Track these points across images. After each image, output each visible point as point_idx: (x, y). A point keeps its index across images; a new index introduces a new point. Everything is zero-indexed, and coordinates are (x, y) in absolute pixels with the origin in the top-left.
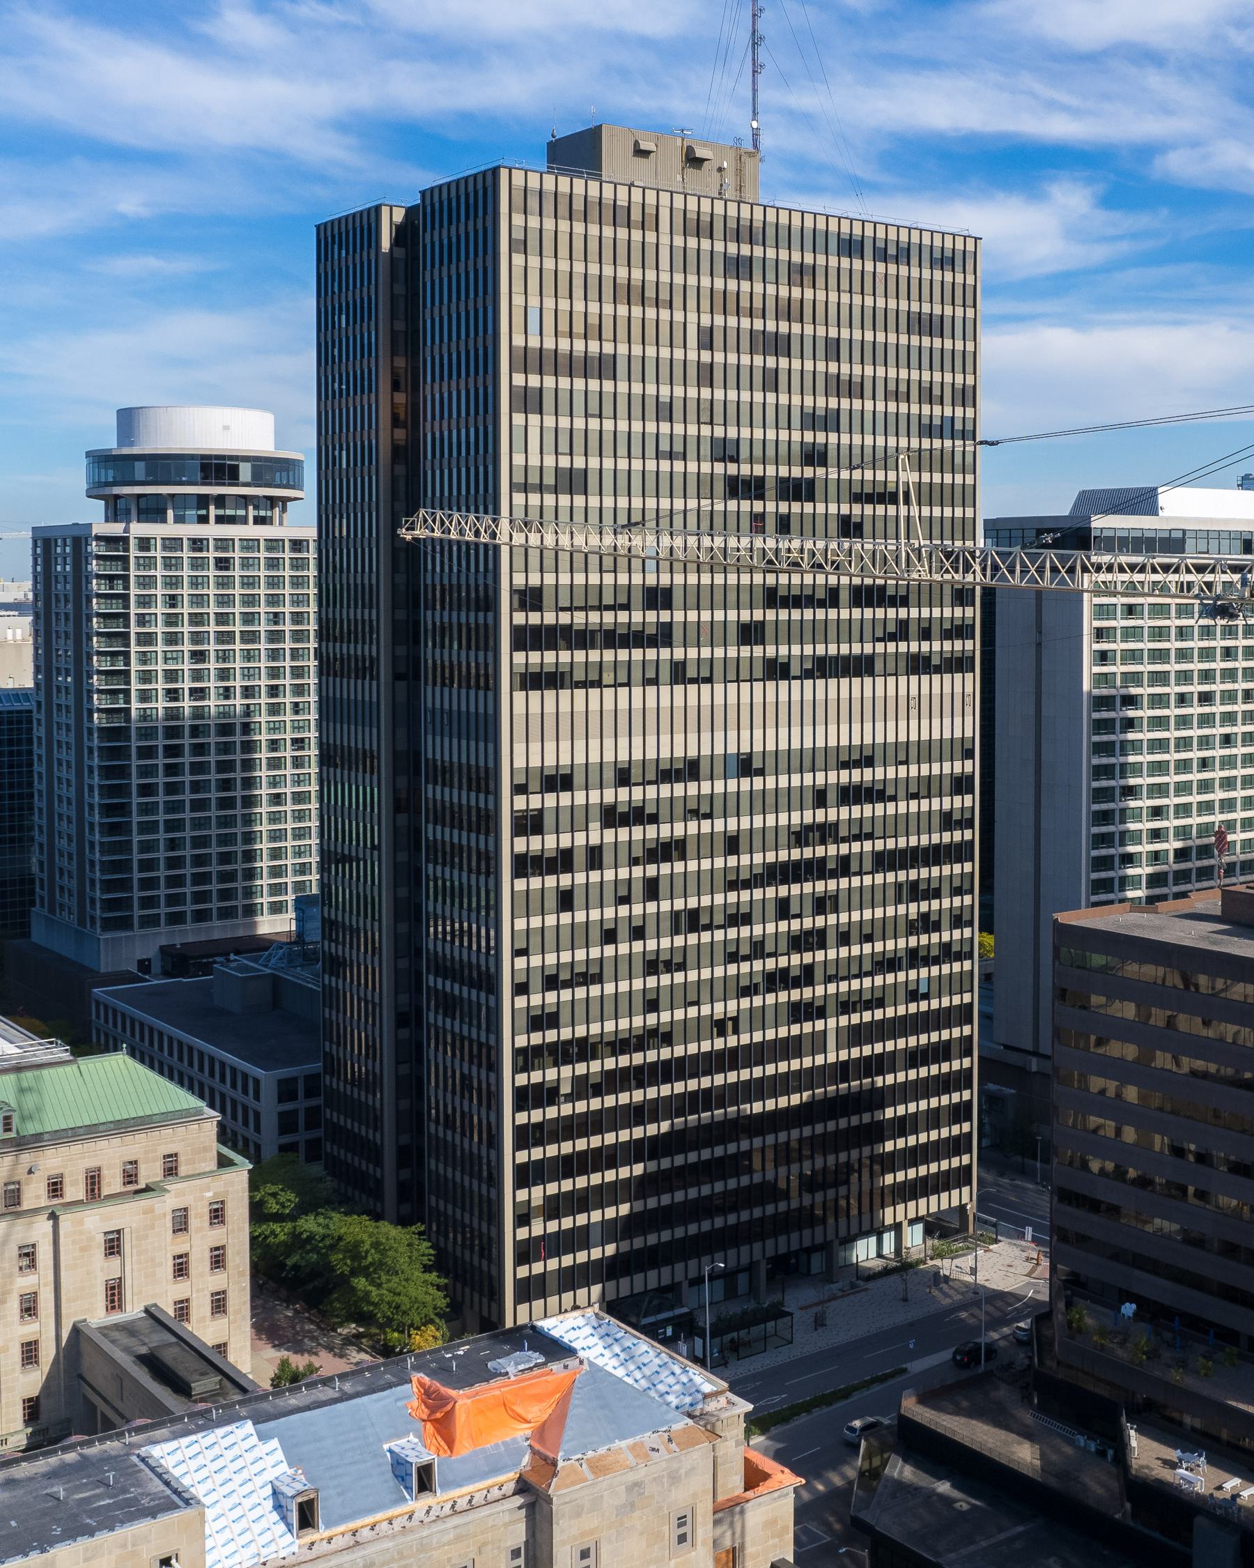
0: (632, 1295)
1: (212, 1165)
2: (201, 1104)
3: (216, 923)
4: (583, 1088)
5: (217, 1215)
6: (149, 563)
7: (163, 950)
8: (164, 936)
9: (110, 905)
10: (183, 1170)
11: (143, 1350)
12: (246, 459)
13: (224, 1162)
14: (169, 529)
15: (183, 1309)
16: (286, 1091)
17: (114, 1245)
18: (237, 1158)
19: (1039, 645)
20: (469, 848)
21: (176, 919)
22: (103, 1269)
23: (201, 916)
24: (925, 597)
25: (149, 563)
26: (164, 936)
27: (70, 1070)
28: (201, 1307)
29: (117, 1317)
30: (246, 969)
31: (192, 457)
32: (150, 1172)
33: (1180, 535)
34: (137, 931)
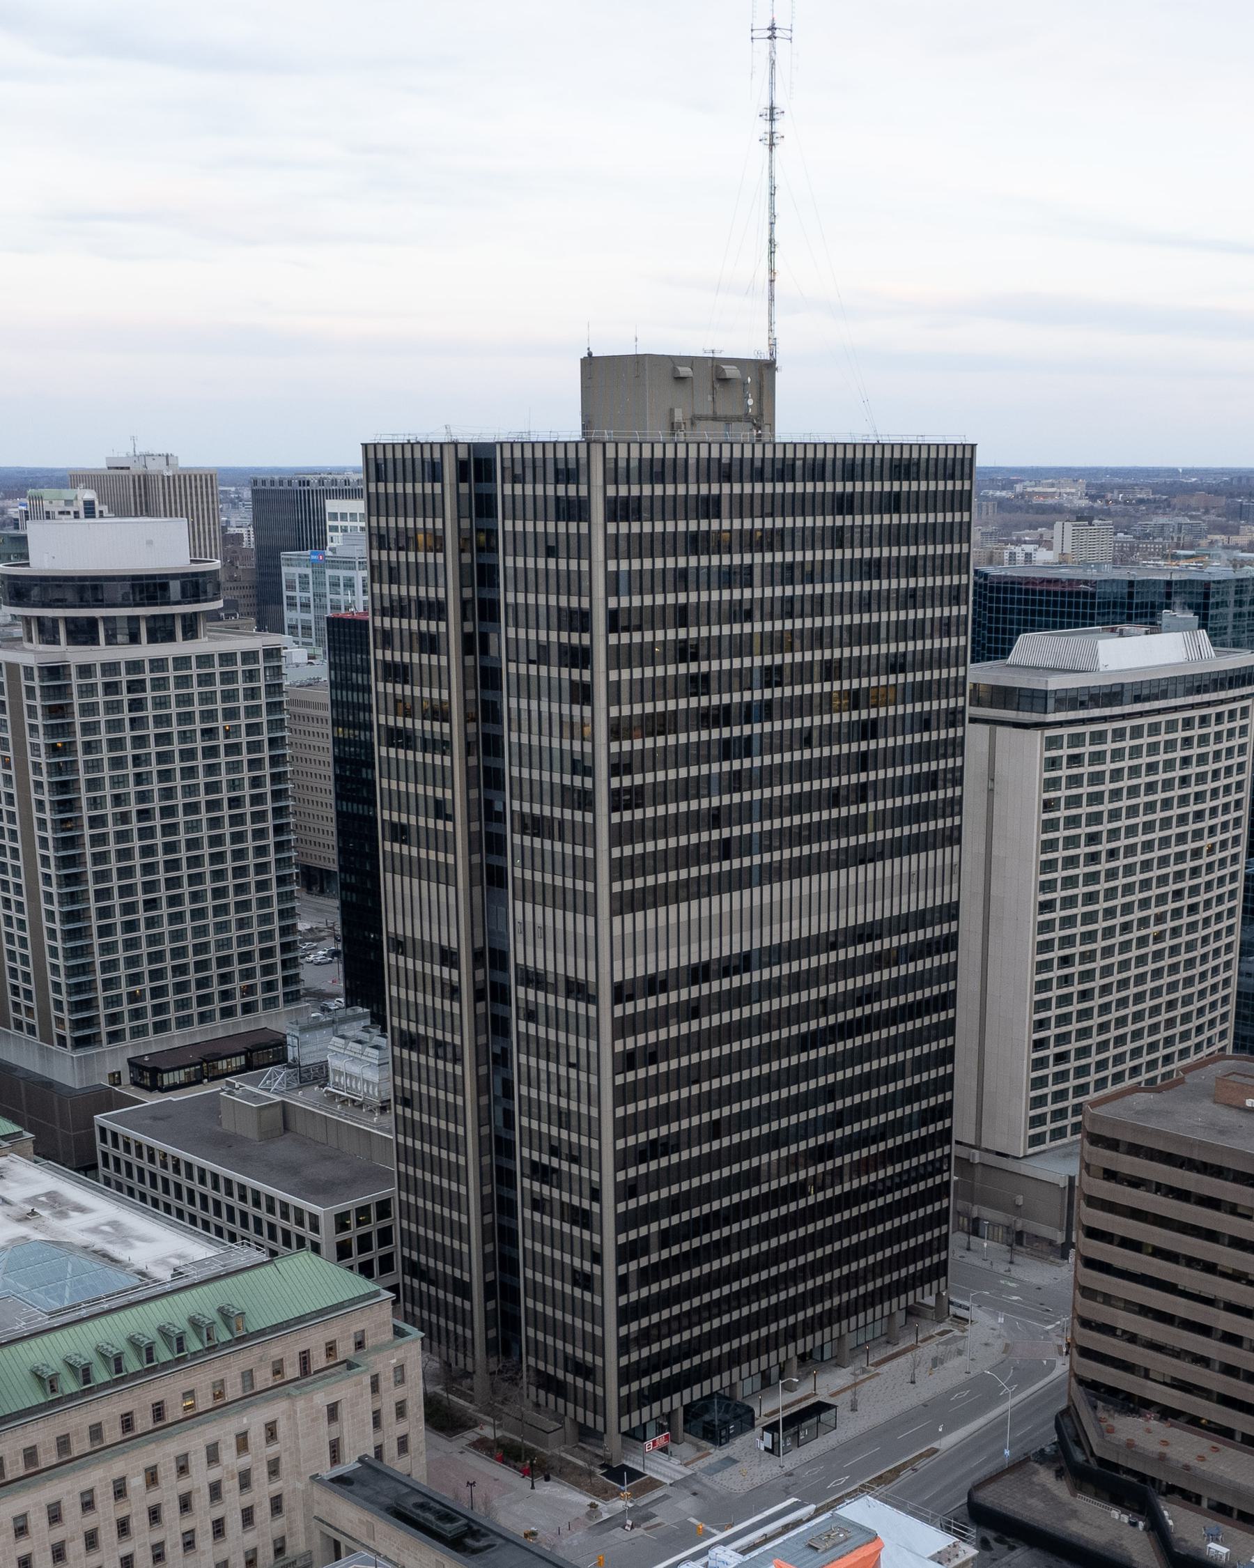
0: (702, 1398)
1: (389, 1335)
2: (17, 1129)
3: (175, 1032)
4: (667, 1238)
5: (400, 1379)
6: (89, 690)
7: (132, 1063)
8: (130, 1048)
9: (77, 1024)
10: (369, 1343)
11: (388, 1501)
12: (175, 576)
13: (399, 1332)
14: (99, 654)
15: (379, 1450)
16: (341, 1222)
17: (333, 1412)
18: (407, 1327)
19: (991, 791)
20: (568, 1047)
21: (138, 1032)
22: (325, 1433)
23: (161, 1027)
24: (669, 505)
25: (89, 690)
26: (130, 1048)
27: (269, 1269)
28: (391, 1449)
29: (340, 1470)
30: (256, 1097)
31: (123, 578)
32: (346, 1349)
33: (1118, 689)
34: (106, 1047)
